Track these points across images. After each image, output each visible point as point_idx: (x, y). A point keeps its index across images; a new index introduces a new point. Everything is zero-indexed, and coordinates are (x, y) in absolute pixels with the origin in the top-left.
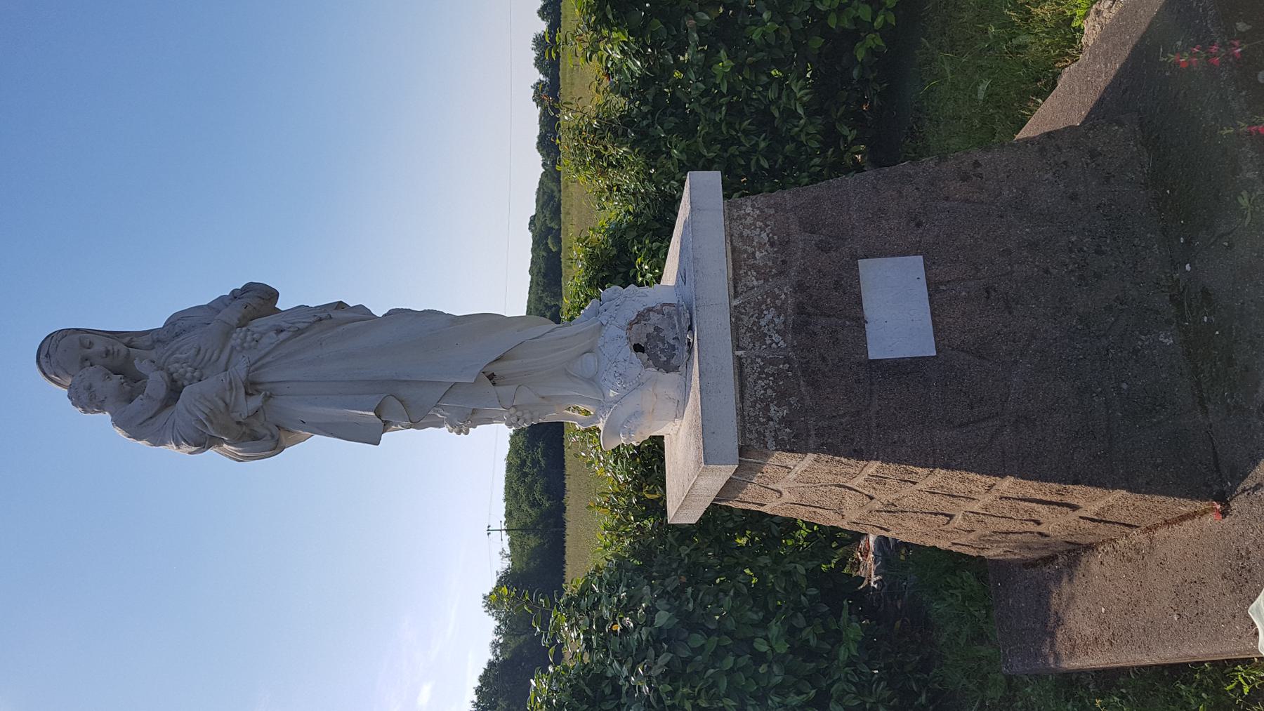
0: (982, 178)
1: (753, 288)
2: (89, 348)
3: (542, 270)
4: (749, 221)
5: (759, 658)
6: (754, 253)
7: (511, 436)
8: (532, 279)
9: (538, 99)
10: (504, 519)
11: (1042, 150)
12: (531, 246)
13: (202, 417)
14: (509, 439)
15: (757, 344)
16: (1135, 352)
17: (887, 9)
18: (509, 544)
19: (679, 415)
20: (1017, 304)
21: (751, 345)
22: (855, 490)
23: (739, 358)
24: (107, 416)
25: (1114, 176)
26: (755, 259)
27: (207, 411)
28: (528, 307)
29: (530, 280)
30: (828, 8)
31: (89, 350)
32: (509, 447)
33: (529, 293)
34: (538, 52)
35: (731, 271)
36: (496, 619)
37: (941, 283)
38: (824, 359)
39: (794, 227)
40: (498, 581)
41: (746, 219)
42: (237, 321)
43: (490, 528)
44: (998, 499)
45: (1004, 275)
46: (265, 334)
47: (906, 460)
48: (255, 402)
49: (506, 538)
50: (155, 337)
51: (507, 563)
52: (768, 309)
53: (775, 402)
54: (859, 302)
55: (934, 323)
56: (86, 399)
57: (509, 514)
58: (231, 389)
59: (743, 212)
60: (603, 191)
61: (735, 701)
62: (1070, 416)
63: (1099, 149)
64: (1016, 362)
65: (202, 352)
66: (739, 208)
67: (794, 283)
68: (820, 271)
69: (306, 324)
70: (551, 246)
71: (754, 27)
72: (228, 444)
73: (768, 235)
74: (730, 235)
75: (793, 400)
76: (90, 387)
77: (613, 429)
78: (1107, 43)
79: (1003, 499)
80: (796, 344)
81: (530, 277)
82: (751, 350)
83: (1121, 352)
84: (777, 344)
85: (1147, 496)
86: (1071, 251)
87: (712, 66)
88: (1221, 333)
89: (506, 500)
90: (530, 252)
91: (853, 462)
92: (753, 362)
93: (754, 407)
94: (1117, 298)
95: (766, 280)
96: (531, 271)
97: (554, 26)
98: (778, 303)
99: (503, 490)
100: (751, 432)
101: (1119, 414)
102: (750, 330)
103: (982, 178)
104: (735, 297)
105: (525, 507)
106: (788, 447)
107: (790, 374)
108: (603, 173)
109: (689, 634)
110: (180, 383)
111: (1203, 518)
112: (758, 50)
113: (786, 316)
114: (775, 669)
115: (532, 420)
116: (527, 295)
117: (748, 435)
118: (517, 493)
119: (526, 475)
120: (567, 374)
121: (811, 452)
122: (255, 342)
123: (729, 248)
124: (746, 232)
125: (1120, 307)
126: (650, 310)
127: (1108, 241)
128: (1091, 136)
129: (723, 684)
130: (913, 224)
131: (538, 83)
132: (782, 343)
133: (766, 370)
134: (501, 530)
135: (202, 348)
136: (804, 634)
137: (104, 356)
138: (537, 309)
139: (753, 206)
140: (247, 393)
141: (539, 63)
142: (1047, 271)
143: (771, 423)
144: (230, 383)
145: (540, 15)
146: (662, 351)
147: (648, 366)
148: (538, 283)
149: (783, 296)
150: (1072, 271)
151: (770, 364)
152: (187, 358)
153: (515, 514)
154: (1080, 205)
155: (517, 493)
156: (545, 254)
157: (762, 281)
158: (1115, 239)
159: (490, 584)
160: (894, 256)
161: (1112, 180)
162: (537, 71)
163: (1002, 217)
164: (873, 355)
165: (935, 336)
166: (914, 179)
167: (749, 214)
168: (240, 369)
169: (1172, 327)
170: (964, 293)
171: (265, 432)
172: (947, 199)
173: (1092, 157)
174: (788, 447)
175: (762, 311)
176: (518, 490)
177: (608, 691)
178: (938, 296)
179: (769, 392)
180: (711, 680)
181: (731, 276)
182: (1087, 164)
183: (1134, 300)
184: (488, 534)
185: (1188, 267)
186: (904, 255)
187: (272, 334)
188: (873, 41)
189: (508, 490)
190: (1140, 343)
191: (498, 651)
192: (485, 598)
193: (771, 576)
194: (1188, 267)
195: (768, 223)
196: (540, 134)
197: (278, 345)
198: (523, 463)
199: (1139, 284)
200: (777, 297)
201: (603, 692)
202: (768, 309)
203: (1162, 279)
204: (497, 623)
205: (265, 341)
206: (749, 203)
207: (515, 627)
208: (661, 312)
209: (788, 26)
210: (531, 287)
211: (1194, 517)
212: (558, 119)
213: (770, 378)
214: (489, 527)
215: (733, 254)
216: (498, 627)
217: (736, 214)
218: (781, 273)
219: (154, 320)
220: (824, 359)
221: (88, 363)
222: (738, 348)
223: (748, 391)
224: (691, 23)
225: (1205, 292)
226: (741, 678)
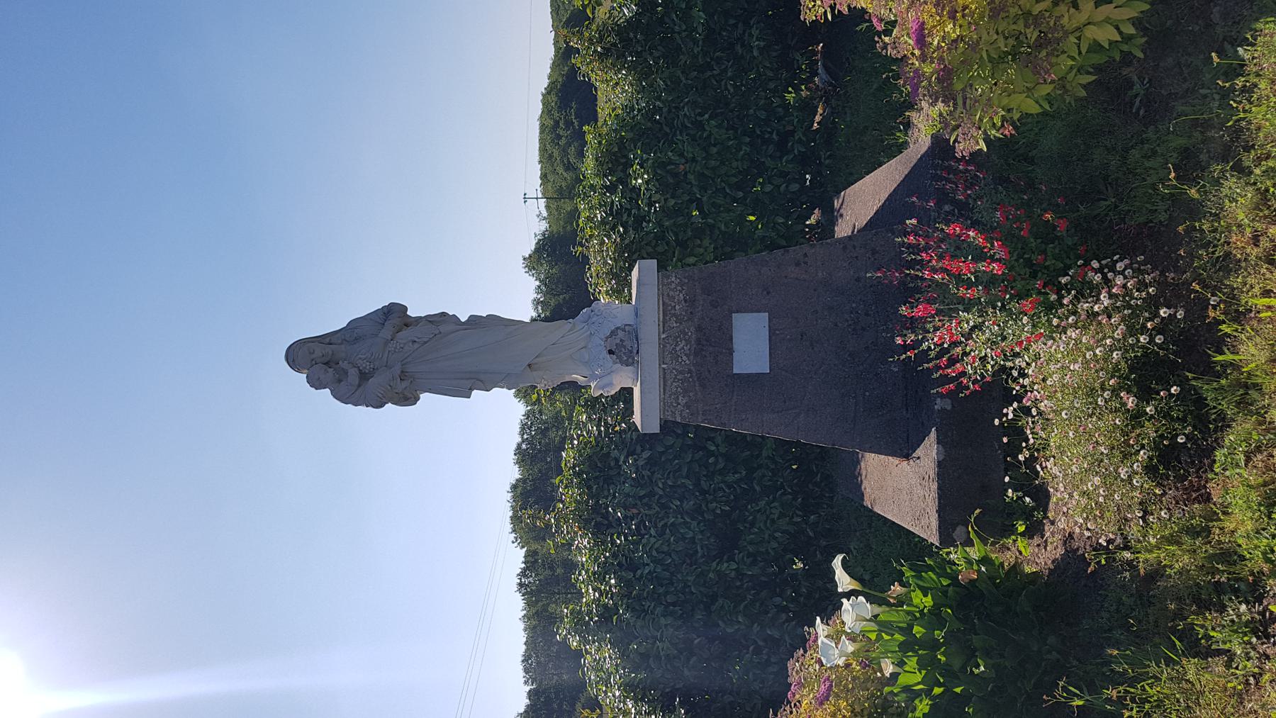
4: (673, 286)
6: (675, 306)
7: (543, 95)
11: (845, 248)
14: (541, 98)
15: (674, 362)
18: (546, 206)
23: (664, 369)
24: (328, 390)
27: (382, 392)
32: (541, 107)
36: (536, 280)
37: (777, 330)
40: (537, 244)
43: (527, 196)
48: (404, 384)
49: (542, 202)
51: (544, 226)
57: (544, 177)
66: (668, 277)
68: (711, 319)
75: (691, 394)
76: (319, 378)
89: (540, 162)
92: (671, 372)
93: (670, 397)
95: (681, 323)
100: (668, 411)
104: (663, 333)
105: (560, 170)
113: (690, 346)
114: (720, 460)
115: (553, 384)
118: (551, 156)
119: (559, 137)
124: (671, 293)
126: (617, 328)
128: (874, 239)
130: (765, 293)
132: (687, 362)
134: (537, 198)
143: (679, 406)
144: (393, 377)
146: (624, 353)
147: (617, 363)
149: (690, 334)
154: (861, 284)
155: (551, 156)
159: (529, 247)
160: (752, 312)
167: (673, 282)
168: (397, 370)
171: (411, 396)
175: (677, 342)
176: (553, 153)
177: (612, 464)
179: (679, 389)
180: (678, 466)
181: (661, 320)
182: (869, 258)
183: (881, 344)
184: (525, 202)
187: (410, 344)
191: (540, 308)
192: (524, 259)
195: (684, 288)
198: (557, 123)
200: (687, 334)
201: (610, 464)
204: (538, 283)
207: (554, 287)
208: (624, 330)
214: (525, 194)
216: (539, 287)
218: (689, 319)
222: (664, 363)
223: (668, 388)
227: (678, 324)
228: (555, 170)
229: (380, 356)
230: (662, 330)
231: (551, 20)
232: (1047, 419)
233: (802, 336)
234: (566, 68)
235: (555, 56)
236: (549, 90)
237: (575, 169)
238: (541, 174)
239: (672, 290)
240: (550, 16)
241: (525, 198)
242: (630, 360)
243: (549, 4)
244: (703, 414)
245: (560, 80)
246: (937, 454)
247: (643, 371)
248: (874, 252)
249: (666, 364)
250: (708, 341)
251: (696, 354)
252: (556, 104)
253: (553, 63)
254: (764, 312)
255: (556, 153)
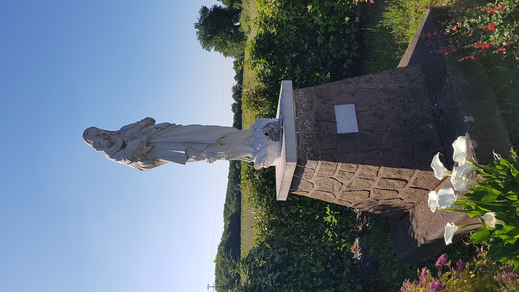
0: (372, 82)
1: (302, 114)
2: (99, 132)
3: (233, 176)
4: (301, 95)
5: (313, 275)
6: (302, 104)
8: (229, 180)
9: (234, 110)
10: (215, 283)
12: (229, 167)
13: (133, 151)
14: (218, 247)
16: (421, 130)
17: (354, 51)
19: (279, 156)
20: (384, 117)
21: (301, 130)
22: (337, 180)
23: (298, 134)
25: (414, 81)
26: (302, 106)
27: (135, 149)
28: (227, 192)
29: (228, 181)
30: (333, 51)
31: (99, 133)
32: (218, 251)
33: (228, 186)
34: (234, 93)
35: (295, 110)
38: (324, 134)
39: (315, 97)
41: (300, 95)
42: (144, 125)
43: (209, 286)
44: (381, 179)
45: (380, 109)
46: (152, 129)
47: (349, 162)
48: (149, 148)
50: (117, 132)
52: (306, 120)
53: (309, 146)
54: (335, 117)
55: (358, 123)
56: (98, 146)
57: (217, 281)
58: (142, 143)
59: (299, 93)
60: (257, 116)
61: (304, 291)
62: (401, 148)
63: (409, 73)
64: (383, 134)
65: (133, 134)
66: (298, 92)
67: (315, 113)
69: (165, 127)
70: (237, 167)
71: (308, 58)
72: (140, 161)
73: (307, 99)
74: (295, 99)
75: (314, 145)
76: (99, 142)
77: (259, 162)
78: (412, 45)
79: (383, 179)
80: (315, 130)
81: (228, 179)
82: (301, 131)
83: (417, 130)
84: (309, 130)
85: (426, 171)
86: (400, 102)
87: (294, 71)
88: (445, 122)
89: (216, 274)
90: (229, 169)
91: (333, 163)
94: (415, 115)
96: (229, 177)
97: (240, 82)
98: (310, 118)
99: (215, 270)
100: (301, 154)
101: (416, 148)
102: (301, 126)
103: (372, 82)
104: (296, 117)
105: (224, 278)
106: (313, 159)
107: (313, 138)
108: (257, 108)
109: (287, 267)
110: (126, 143)
111: (446, 180)
112: (310, 65)
116: (227, 187)
117: (300, 156)
118: (220, 272)
120: (244, 144)
121: (320, 160)
122: (149, 132)
123: (295, 103)
124: (300, 98)
125: (416, 117)
127: (412, 99)
129: (300, 284)
131: (233, 104)
132: (311, 129)
133: (306, 137)
134: (213, 287)
135: (133, 133)
136: (331, 270)
137: (103, 135)
138: (231, 192)
139: (302, 91)
140: (146, 146)
141: (234, 96)
142: (393, 108)
143: (307, 152)
145: (235, 79)
146: (274, 135)
148: (231, 182)
149: (311, 116)
150: (401, 108)
151: (307, 135)
152: (128, 136)
153: (220, 281)
155: (220, 272)
156: (234, 170)
157: (305, 112)
158: (414, 98)
160: (345, 104)
161: (413, 82)
162: (233, 99)
163: (378, 93)
164: (339, 132)
165: (358, 127)
166: (351, 83)
168: (145, 138)
169: (433, 123)
170: (367, 114)
172: (362, 88)
173: (407, 76)
174: (313, 159)
175: (305, 120)
176: (221, 270)
178: (359, 115)
179: (307, 143)
181: (295, 111)
182: (405, 78)
184: (208, 288)
185: (436, 104)
186: (349, 104)
188: (349, 61)
189: (217, 270)
190: (423, 128)
193: (318, 248)
194: (436, 104)
195: (307, 96)
196: (234, 123)
197: (156, 132)
199: (422, 111)
200: (309, 116)
202: (306, 120)
203: (429, 109)
205: (152, 131)
206: (301, 90)
209: (320, 57)
210: (228, 184)
211: (443, 181)
212: (242, 92)
213: (307, 139)
214: (208, 285)
215: (296, 104)
217: (297, 93)
219: (117, 128)
220: (324, 134)
221: (99, 136)
222: (297, 131)
224: (286, 57)
225: (441, 111)
226: (306, 282)
227: (304, 112)
228: (222, 278)
229: (137, 136)
230: (295, 115)
231: (224, 219)
232: (511, 234)
233: (375, 114)
234: (229, 235)
235: (225, 231)
236: (221, 244)
237: (230, 277)
238: (215, 280)
239: (301, 97)
240: (223, 217)
241: (208, 287)
242: (277, 138)
243: (223, 213)
244: (321, 155)
245: (226, 240)
246: (473, 145)
247: (286, 131)
248: (407, 75)
249: (298, 131)
250: (322, 119)
251: (315, 126)
252: (224, 249)
253: (224, 233)
254: (352, 104)
255: (222, 270)
